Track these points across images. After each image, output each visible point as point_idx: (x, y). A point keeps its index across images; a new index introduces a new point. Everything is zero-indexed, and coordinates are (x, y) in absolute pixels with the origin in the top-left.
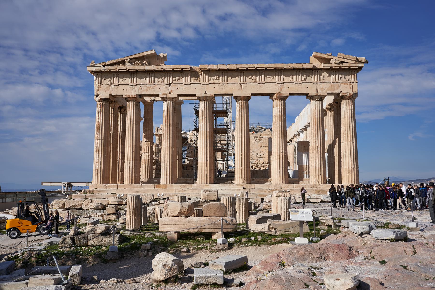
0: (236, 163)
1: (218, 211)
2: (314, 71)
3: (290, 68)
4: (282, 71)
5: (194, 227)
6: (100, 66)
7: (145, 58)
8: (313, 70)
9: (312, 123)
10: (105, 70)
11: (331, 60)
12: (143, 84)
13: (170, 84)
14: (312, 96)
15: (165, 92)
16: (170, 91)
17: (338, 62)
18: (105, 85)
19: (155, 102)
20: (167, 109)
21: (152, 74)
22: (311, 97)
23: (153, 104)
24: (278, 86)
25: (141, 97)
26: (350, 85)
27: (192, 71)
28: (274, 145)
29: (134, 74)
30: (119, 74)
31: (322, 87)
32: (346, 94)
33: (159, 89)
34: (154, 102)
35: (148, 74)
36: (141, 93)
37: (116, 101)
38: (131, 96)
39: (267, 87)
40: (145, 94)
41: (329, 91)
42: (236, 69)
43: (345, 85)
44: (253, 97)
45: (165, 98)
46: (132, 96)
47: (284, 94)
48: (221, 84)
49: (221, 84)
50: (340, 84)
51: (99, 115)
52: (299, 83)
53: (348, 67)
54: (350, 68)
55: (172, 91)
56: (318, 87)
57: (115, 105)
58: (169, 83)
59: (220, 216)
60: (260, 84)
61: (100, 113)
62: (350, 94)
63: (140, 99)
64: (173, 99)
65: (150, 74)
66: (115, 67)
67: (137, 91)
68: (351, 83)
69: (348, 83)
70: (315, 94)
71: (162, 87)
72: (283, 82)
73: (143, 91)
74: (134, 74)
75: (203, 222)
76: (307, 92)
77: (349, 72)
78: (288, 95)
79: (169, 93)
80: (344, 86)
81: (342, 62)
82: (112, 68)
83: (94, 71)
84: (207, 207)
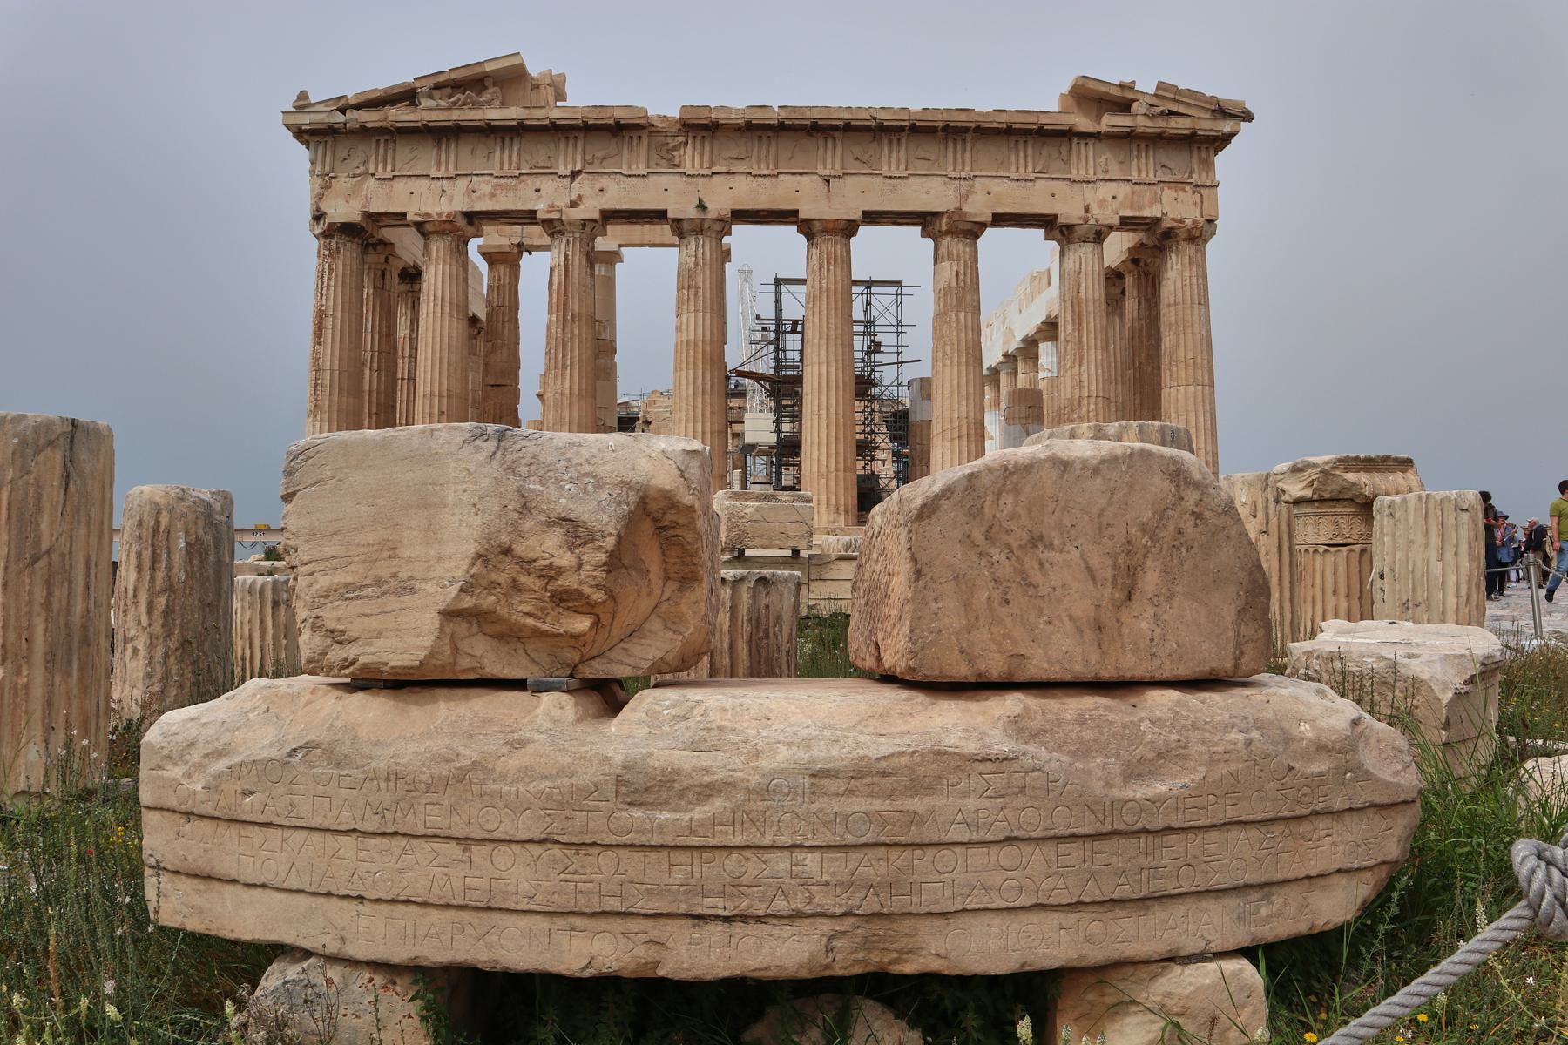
0: (808, 454)
1: (1151, 580)
2: (1075, 140)
3: (995, 125)
4: (969, 137)
5: (732, 887)
6: (329, 109)
7: (487, 83)
8: (1070, 140)
9: (1069, 318)
10: (345, 124)
11: (1135, 105)
12: (477, 175)
13: (574, 174)
14: (1070, 227)
15: (556, 203)
16: (574, 197)
17: (1158, 110)
18: (347, 179)
19: (525, 254)
20: (563, 263)
21: (512, 139)
22: (1064, 229)
25: (470, 223)
26: (1194, 192)
27: (653, 129)
28: (940, 391)
29: (448, 140)
30: (395, 142)
31: (1101, 197)
32: (1180, 221)
33: (538, 191)
34: (520, 253)
35: (499, 140)
38: (436, 217)
40: (484, 209)
42: (808, 122)
43: (1176, 191)
45: (556, 224)
46: (440, 215)
47: (976, 215)
48: (755, 176)
49: (755, 176)
50: (1162, 190)
52: (1026, 180)
53: (1187, 132)
54: (1194, 134)
55: (580, 197)
56: (1091, 195)
57: (387, 258)
58: (572, 172)
59: (1183, 671)
60: (890, 177)
61: (326, 278)
62: (1194, 222)
63: (469, 227)
64: (584, 225)
65: (503, 140)
66: (382, 113)
68: (1197, 186)
69: (1187, 188)
70: (1080, 218)
71: (548, 185)
72: (972, 174)
73: (479, 198)
74: (448, 140)
75: (919, 804)
76: (1054, 212)
77: (1191, 153)
78: (988, 218)
79: (571, 207)
80: (1175, 195)
81: (1172, 113)
82: (370, 118)
83: (308, 127)
84: (975, 513)
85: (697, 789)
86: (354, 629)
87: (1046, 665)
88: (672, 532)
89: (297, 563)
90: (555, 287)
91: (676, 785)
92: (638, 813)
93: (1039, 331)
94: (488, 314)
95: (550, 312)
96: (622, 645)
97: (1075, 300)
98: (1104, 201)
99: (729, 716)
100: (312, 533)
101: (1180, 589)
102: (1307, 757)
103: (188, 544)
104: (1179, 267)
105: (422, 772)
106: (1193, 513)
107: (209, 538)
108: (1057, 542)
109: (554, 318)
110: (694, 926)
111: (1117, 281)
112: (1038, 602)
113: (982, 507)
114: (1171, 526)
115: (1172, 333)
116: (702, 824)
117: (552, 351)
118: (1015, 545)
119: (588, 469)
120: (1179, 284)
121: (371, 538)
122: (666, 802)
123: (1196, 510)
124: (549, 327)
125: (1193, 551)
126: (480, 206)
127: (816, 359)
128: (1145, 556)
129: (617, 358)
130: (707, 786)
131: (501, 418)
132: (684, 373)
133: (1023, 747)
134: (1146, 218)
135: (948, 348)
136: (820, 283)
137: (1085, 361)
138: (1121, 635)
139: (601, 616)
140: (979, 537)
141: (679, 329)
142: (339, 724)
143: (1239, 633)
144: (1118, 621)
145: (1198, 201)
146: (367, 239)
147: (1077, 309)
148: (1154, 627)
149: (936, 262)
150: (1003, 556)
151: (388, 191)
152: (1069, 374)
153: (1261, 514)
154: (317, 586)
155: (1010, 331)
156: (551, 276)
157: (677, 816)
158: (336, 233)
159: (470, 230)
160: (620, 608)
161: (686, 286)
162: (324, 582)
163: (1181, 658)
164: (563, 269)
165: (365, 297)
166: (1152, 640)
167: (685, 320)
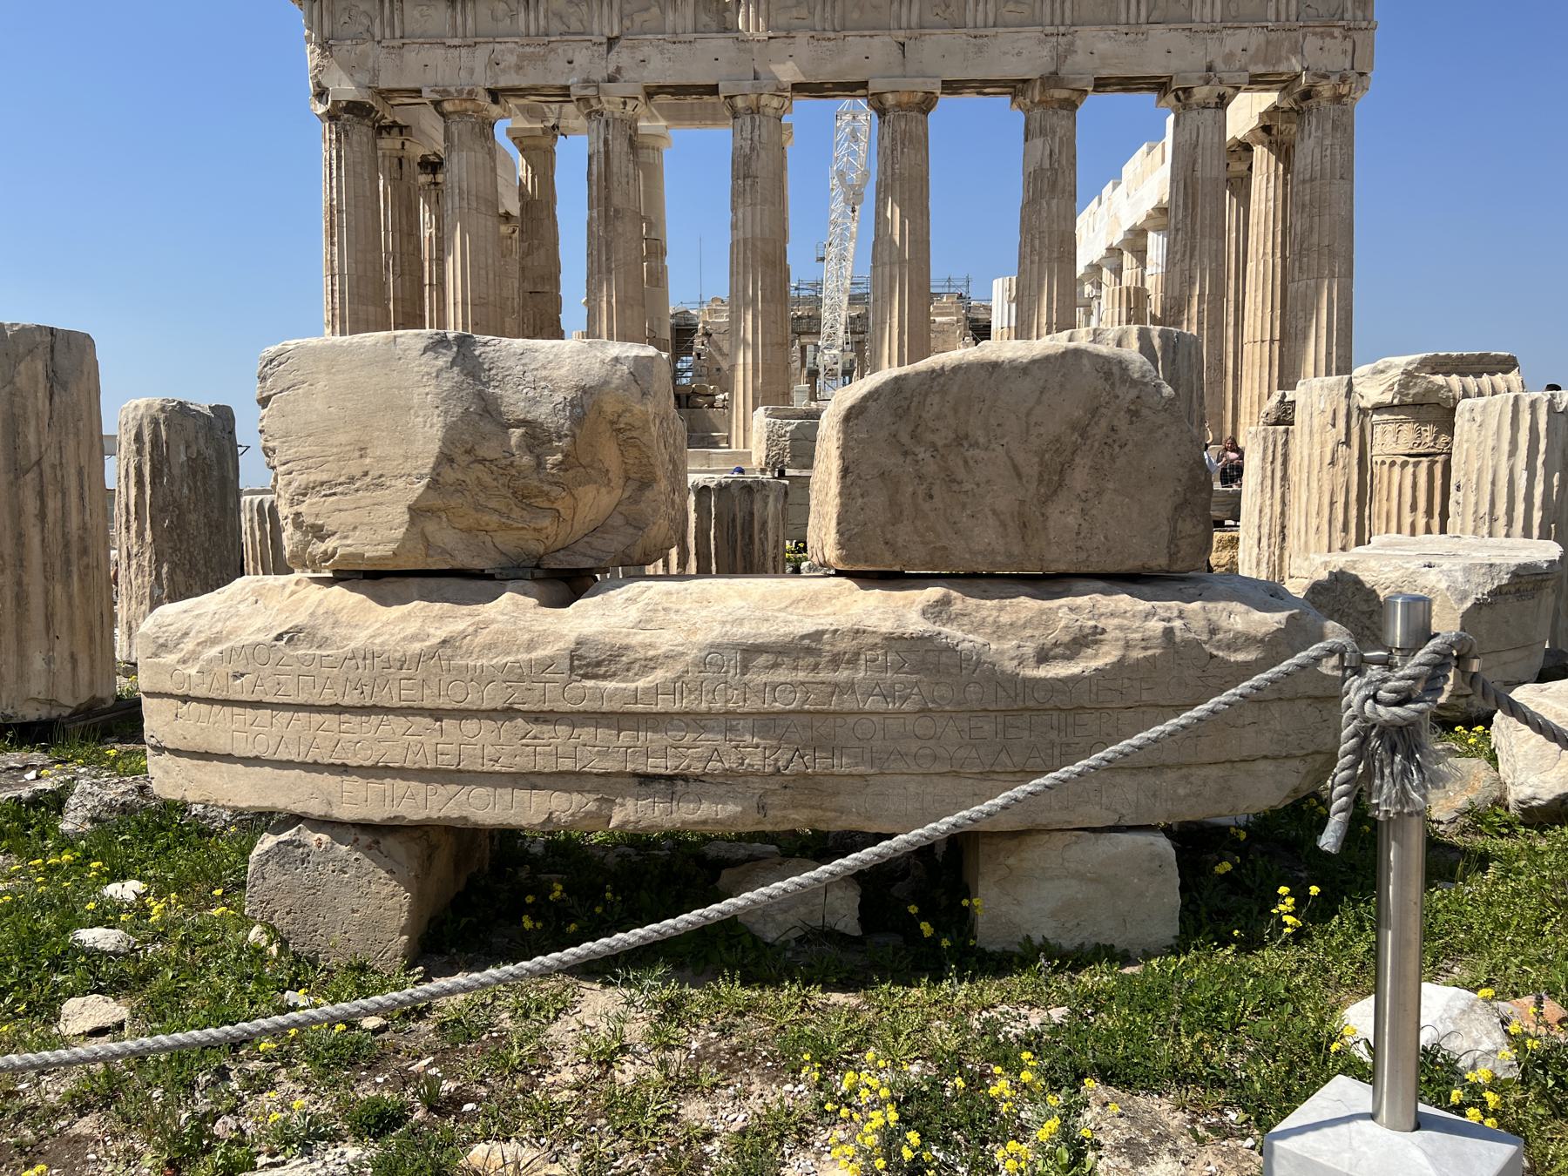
1: (1079, 478)
13: (612, 42)
16: (611, 69)
20: (602, 150)
22: (1180, 93)
23: (552, 147)
24: (1049, 46)
26: (1345, 38)
31: (1227, 50)
33: (570, 62)
36: (497, 82)
37: (406, 127)
39: (1005, 53)
41: (1256, 64)
43: (1322, 38)
44: (945, 102)
51: (334, 174)
55: (618, 69)
57: (403, 144)
61: (334, 167)
67: (477, 70)
73: (504, 71)
79: (609, 82)
80: (1320, 43)
85: (643, 663)
86: (330, 525)
87: (967, 556)
88: (628, 434)
89: (276, 463)
90: (594, 178)
91: (624, 658)
92: (590, 683)
93: (1149, 217)
94: (522, 209)
95: (590, 208)
96: (586, 539)
97: (1189, 181)
98: (1231, 55)
99: (674, 599)
100: (287, 435)
101: (1111, 485)
102: (1232, 646)
103: (189, 458)
104: (1319, 134)
105: (396, 651)
106: (1129, 411)
107: (209, 452)
108: (982, 440)
109: (595, 215)
110: (640, 784)
111: (1244, 155)
112: (963, 498)
113: (909, 408)
114: (1104, 423)
115: (1305, 215)
116: (646, 691)
117: (595, 253)
118: (940, 444)
119: (544, 373)
120: (1317, 155)
121: (343, 438)
122: (614, 675)
123: (1132, 407)
124: (589, 225)
125: (1126, 449)
126: (502, 84)
127: (886, 259)
128: (1074, 453)
129: (668, 261)
130: (651, 660)
131: (541, 329)
132: (741, 277)
133: (937, 628)
134: (1281, 74)
135: (1037, 242)
136: (893, 169)
137: (1197, 253)
138: (1045, 528)
139: (561, 510)
140: (905, 438)
141: (734, 227)
142: (321, 611)
143: (1175, 529)
144: (1043, 515)
145: (1350, 50)
146: (378, 121)
147: (1190, 191)
148: (1082, 521)
149: (1026, 140)
150: (928, 454)
151: (398, 62)
152: (1178, 268)
153: (1341, 424)
154: (295, 484)
155: (1116, 219)
156: (590, 165)
157: (623, 685)
158: (347, 115)
159: (495, 110)
160: (580, 505)
161: (741, 176)
162: (300, 480)
163: (1109, 551)
164: (602, 156)
165: (381, 189)
166: (1078, 534)
167: (740, 215)
